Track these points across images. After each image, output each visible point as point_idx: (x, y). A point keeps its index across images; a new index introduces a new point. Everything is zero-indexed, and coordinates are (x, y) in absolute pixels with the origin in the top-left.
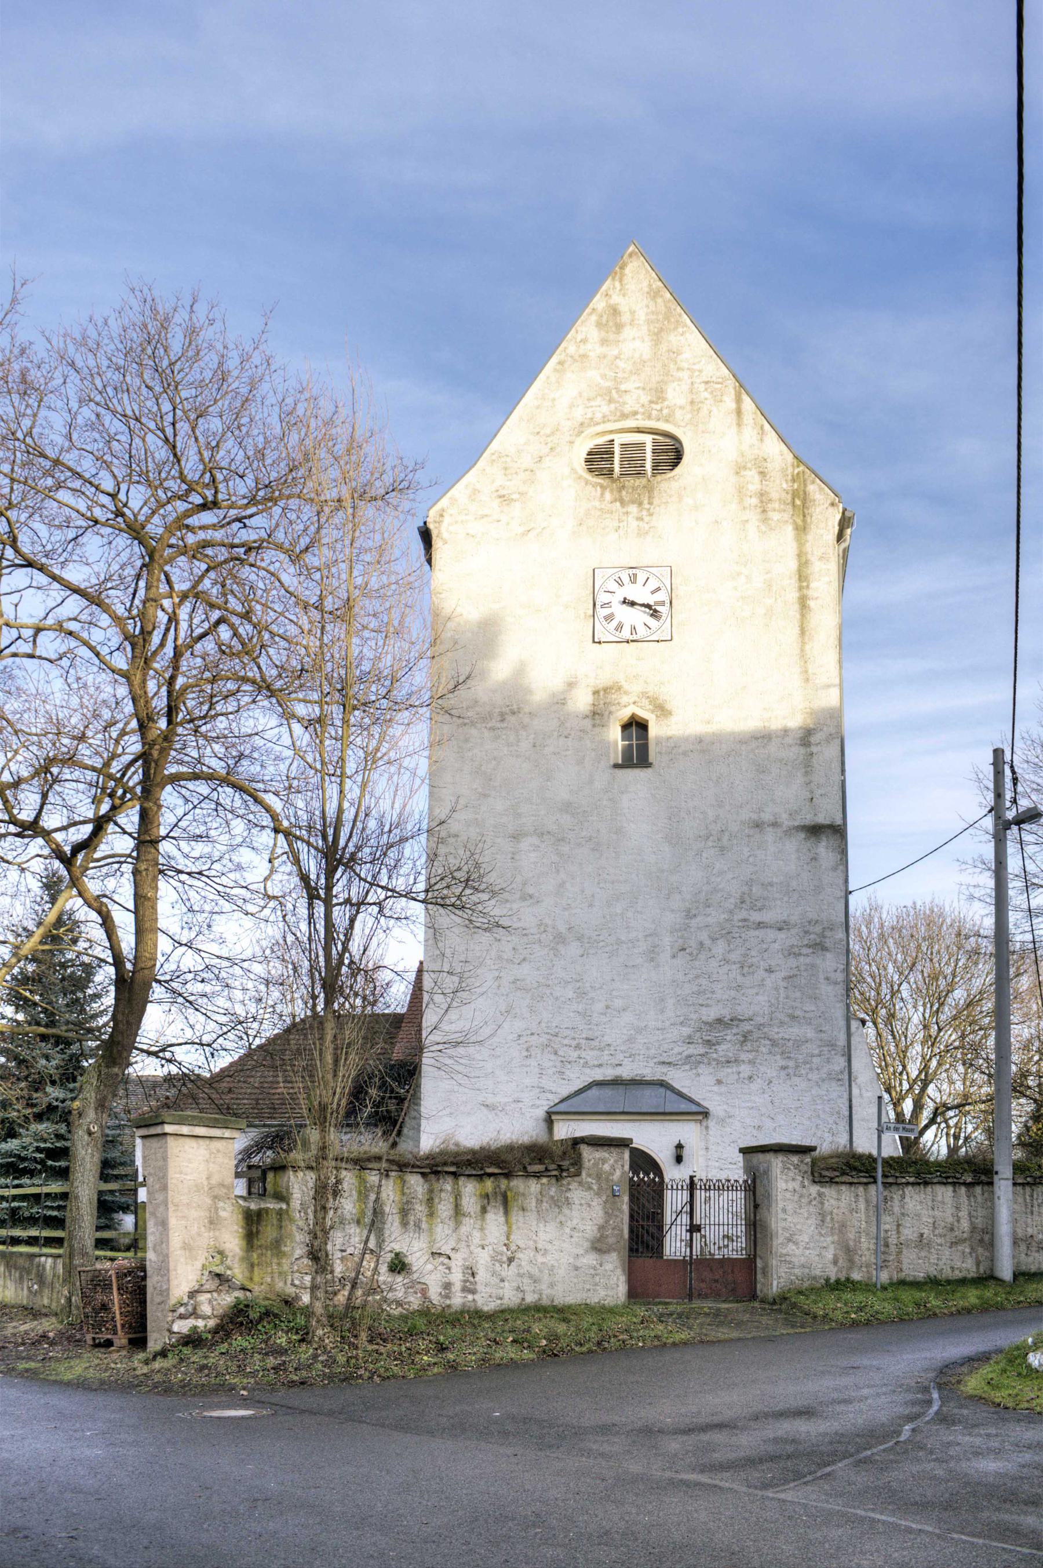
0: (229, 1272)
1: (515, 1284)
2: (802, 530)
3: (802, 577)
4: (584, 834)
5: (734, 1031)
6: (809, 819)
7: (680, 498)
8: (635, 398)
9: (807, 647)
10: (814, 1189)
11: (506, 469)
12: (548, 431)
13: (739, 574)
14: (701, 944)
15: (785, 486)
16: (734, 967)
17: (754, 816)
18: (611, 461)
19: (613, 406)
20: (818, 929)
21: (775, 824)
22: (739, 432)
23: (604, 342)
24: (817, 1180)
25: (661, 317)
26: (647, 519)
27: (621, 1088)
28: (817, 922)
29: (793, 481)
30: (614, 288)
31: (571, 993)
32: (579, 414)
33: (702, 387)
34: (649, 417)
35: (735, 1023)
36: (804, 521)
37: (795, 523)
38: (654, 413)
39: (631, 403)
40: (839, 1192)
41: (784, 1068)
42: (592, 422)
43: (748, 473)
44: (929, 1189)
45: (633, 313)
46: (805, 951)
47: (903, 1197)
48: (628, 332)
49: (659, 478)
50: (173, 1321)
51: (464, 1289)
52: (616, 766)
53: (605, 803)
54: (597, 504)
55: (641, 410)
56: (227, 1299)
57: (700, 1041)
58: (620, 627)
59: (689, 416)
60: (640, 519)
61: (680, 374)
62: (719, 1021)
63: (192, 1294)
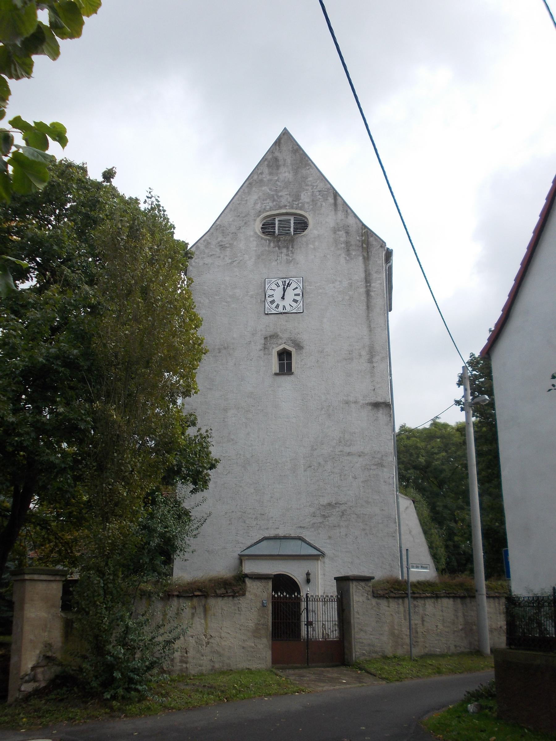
0: (54, 655)
1: (209, 658)
2: (366, 259)
3: (368, 280)
4: (259, 408)
5: (337, 509)
6: (373, 399)
7: (307, 244)
8: (285, 198)
9: (370, 315)
10: (374, 601)
11: (223, 233)
12: (243, 215)
13: (336, 280)
14: (319, 463)
15: (358, 238)
16: (336, 476)
17: (345, 398)
18: (274, 228)
19: (275, 203)
20: (379, 456)
21: (356, 402)
22: (336, 214)
23: (271, 174)
24: (375, 595)
25: (298, 162)
26: (291, 255)
27: (279, 541)
28: (378, 452)
29: (362, 236)
30: (276, 149)
31: (253, 490)
32: (258, 207)
33: (318, 193)
34: (292, 208)
35: (338, 505)
36: (368, 255)
37: (363, 256)
38: (295, 205)
39: (283, 201)
40: (389, 602)
41: (364, 530)
42: (265, 210)
43: (340, 233)
44: (439, 600)
45: (285, 160)
46: (373, 467)
47: (425, 605)
48: (282, 169)
49: (297, 236)
50: (22, 685)
51: (182, 661)
52: (276, 374)
53: (270, 392)
54: (267, 248)
55: (288, 204)
56: (55, 670)
57: (320, 515)
58: (277, 306)
59: (311, 207)
60: (287, 255)
61: (307, 188)
62: (330, 504)
63: (33, 668)
